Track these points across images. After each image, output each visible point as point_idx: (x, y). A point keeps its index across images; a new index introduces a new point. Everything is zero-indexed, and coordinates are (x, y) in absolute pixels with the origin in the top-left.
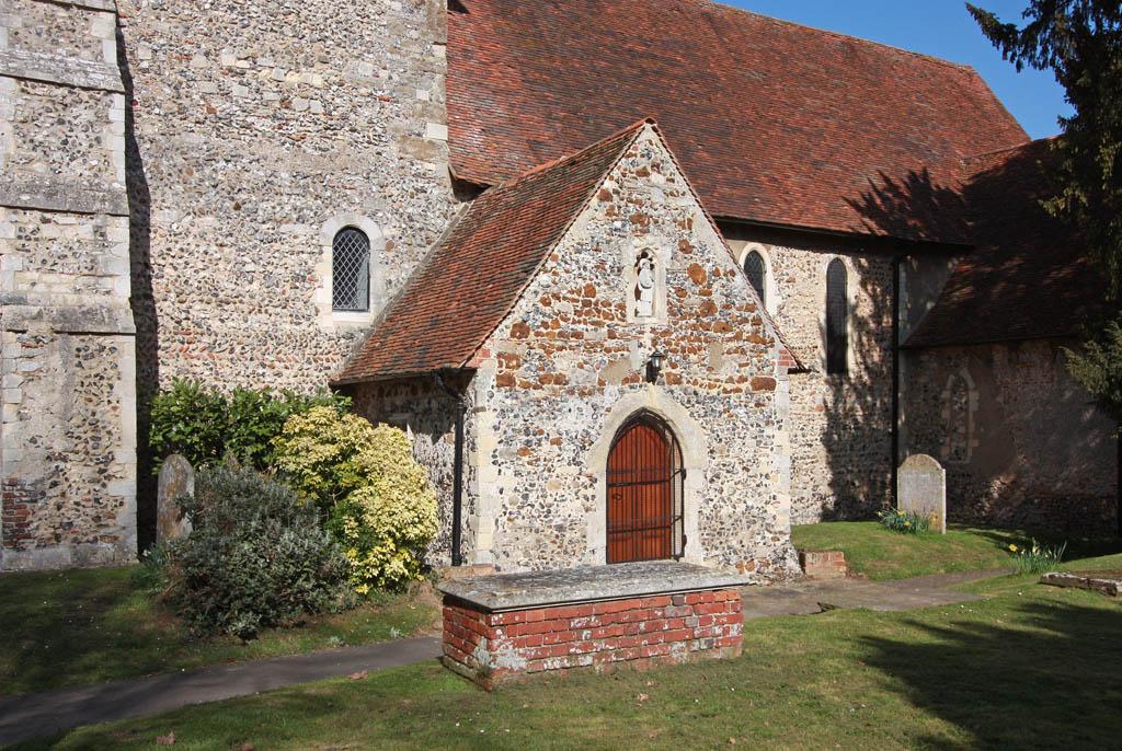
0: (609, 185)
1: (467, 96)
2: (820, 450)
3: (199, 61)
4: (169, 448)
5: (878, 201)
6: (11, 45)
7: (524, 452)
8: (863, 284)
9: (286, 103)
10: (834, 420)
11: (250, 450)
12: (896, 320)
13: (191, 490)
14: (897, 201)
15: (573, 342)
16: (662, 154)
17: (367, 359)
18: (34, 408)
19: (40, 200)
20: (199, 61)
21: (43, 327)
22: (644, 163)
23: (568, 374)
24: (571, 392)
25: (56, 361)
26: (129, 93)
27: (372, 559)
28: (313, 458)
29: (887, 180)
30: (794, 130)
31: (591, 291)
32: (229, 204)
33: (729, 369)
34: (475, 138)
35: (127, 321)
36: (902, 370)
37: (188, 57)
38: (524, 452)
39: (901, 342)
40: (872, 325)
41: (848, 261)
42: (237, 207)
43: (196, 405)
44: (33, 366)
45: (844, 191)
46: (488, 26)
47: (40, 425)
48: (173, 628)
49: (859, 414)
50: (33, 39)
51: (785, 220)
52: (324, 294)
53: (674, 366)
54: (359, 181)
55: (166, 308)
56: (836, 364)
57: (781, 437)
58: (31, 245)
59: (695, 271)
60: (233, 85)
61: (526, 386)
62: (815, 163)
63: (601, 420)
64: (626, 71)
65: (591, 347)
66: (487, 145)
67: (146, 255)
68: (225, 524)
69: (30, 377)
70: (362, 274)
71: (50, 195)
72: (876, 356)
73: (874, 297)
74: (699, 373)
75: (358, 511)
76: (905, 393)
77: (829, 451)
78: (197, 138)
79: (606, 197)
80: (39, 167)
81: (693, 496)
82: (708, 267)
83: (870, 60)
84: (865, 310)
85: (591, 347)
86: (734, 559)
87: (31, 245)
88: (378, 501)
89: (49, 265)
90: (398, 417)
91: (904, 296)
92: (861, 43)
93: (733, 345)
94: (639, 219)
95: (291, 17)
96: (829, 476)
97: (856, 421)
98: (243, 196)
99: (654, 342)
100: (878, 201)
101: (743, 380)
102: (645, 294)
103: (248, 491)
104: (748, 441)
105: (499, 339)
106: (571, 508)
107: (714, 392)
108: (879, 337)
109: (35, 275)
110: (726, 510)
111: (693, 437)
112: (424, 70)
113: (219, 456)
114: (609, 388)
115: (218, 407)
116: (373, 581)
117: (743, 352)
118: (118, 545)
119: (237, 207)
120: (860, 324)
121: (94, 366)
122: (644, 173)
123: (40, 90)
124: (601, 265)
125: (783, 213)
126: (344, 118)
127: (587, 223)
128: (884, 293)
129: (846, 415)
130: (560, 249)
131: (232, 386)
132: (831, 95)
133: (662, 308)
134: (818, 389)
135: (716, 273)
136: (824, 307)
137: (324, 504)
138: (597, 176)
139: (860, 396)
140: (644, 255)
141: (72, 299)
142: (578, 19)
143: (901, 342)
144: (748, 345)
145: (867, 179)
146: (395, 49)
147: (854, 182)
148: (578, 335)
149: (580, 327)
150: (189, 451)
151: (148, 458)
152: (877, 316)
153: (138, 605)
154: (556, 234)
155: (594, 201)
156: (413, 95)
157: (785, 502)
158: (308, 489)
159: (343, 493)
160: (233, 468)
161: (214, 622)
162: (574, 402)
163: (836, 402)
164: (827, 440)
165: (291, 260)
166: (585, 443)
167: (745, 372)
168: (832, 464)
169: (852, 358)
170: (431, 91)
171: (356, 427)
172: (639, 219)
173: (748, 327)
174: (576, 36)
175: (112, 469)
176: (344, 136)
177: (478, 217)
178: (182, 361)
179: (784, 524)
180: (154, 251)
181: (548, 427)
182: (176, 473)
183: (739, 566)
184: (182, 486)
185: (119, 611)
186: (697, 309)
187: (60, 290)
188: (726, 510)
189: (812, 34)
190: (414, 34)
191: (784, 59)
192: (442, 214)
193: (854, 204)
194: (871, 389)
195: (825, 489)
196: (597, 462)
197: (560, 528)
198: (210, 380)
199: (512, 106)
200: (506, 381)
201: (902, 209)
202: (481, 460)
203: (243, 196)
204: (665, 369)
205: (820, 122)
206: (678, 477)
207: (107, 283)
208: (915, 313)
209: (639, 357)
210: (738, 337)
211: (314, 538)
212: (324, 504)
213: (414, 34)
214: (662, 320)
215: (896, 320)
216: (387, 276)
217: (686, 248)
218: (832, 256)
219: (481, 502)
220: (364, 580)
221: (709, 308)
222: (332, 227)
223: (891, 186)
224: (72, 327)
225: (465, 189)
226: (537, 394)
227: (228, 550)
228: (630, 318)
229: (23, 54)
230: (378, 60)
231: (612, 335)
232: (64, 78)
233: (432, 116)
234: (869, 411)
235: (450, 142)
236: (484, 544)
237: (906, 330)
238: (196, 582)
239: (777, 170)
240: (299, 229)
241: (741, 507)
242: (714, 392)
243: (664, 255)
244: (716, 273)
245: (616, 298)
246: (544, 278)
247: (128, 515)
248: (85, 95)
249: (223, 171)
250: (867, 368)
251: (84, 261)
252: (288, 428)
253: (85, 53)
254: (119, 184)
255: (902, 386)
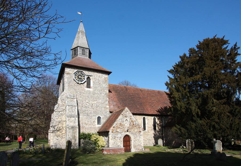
0: (122, 113)
1: (111, 102)
2: (153, 138)
3: (84, 101)
4: (81, 138)
5: (160, 110)
6: (68, 102)
7: (114, 139)
8: (158, 120)
9: (92, 105)
10: (155, 135)
11: (89, 138)
12: (162, 124)
13: (83, 142)
14: (162, 110)
15: (119, 128)
16: (128, 110)
17: (100, 130)
18: (69, 135)
19: (70, 116)
20: (84, 101)
21: (70, 128)
22: (126, 111)
23: (119, 131)
24: (119, 133)
25: (71, 130)
26: (78, 106)
27: (99, 148)
28: (94, 139)
29: (161, 108)
30: (150, 103)
31: (121, 123)
32: (87, 115)
33: (136, 130)
34: (112, 107)
35: (78, 127)
36: (163, 129)
37: (83, 101)
38: (114, 139)
39: (163, 126)
40: (159, 124)
41: (156, 117)
42: (88, 115)
43: (84, 134)
44: (69, 131)
45: (156, 110)
46: (114, 94)
47: (70, 136)
48: (82, 153)
49: (158, 134)
50: (69, 102)
51: (148, 113)
52: (96, 123)
53: (130, 130)
54: (100, 112)
55: (81, 125)
56: (155, 129)
57: (142, 137)
58: (69, 120)
59: (132, 121)
60: (87, 104)
61: (115, 132)
62: (152, 107)
63: (122, 136)
64: (130, 97)
65: (121, 129)
66: (113, 107)
67: (79, 120)
68: (86, 145)
69: (69, 132)
70: (100, 121)
71: (71, 116)
72: (160, 128)
73: (159, 121)
74: (133, 131)
75: (98, 144)
76: (164, 132)
77: (154, 138)
78: (84, 109)
79: (122, 114)
80: (70, 113)
81: (132, 143)
82: (133, 121)
83: (161, 93)
84: (158, 122)
85: (121, 129)
86: (137, 149)
87: (69, 120)
88: (100, 143)
89: (71, 122)
90: (103, 135)
91: (163, 121)
92: (160, 91)
93: (136, 128)
94: (126, 116)
95: (93, 97)
96: (154, 141)
97: (158, 135)
98: (88, 114)
99: (128, 128)
100: (160, 110)
101: (138, 131)
102: (127, 123)
103: (88, 142)
104: (138, 137)
105: (112, 128)
106: (119, 144)
107: (134, 133)
108: (160, 126)
109: (70, 123)
110: (136, 144)
111: (132, 137)
112: (106, 100)
113: (86, 139)
114: (123, 132)
115: (86, 135)
116: (99, 150)
117: (137, 129)
118: (77, 147)
119: (88, 115)
120: (158, 124)
121: (75, 131)
122: (126, 112)
123: (70, 106)
124: (122, 121)
125: (147, 112)
126: (98, 106)
127: (120, 117)
128: (161, 121)
129: (156, 134)
130: (118, 119)
131: (87, 132)
132: (155, 98)
133: (128, 125)
134: (153, 132)
135: (134, 121)
136: (153, 123)
137: (95, 143)
138: (121, 112)
139: (158, 132)
140: (126, 120)
141: (73, 125)
142: (125, 92)
143: (163, 126)
144: (138, 128)
145: (159, 108)
146: (103, 99)
147: (157, 108)
148: (120, 128)
149: (120, 127)
150: (83, 138)
151: (80, 139)
152: (160, 123)
153: (79, 151)
154: (117, 118)
155: (121, 115)
156: (105, 103)
157: (143, 143)
158: (94, 142)
159: (97, 142)
160: (87, 140)
161: (85, 153)
162: (119, 134)
163: (155, 133)
164: (154, 137)
165: (93, 120)
166: (121, 138)
167: (138, 131)
168: (155, 140)
169: (157, 128)
170: (107, 102)
171: (98, 136)
172: (126, 116)
173: (138, 126)
174: (124, 94)
175: (76, 140)
176: (98, 108)
177: (112, 115)
178: (83, 130)
179: (143, 146)
180: (80, 120)
181: (117, 136)
182: (82, 140)
183: (138, 150)
184: (82, 141)
185: (77, 151)
186: (132, 125)
187: (72, 124)
188: (136, 144)
189: (154, 91)
190: (105, 97)
191: (150, 94)
192: (108, 115)
193: (157, 111)
194: (159, 131)
195: (154, 143)
196: (122, 139)
197: (118, 146)
198: (85, 132)
199: (116, 103)
200: (113, 132)
201: (163, 111)
202: (110, 139)
203: (88, 114)
204: (129, 130)
205: (153, 101)
206: (131, 141)
207: (76, 123)
208: (164, 123)
209: (126, 130)
210: (137, 127)
211: (94, 146)
212: (95, 143)
213: (105, 97)
214: (128, 126)
215: (162, 124)
216: (103, 121)
217: (131, 119)
218: (154, 117)
219: (110, 143)
220: (99, 150)
221: (134, 124)
222: (97, 117)
223: (162, 108)
224: (73, 127)
225: (111, 112)
226: (115, 133)
227: (86, 147)
228: (125, 126)
229: (69, 103)
230: (102, 100)
231: (123, 127)
232: (72, 105)
233: (107, 105)
234: (159, 134)
235: (109, 107)
236: (111, 146)
237: (164, 125)
238: (84, 149)
239: (147, 108)
240: (94, 117)
241: (138, 144)
242: (134, 133)
243: (128, 120)
244: (134, 121)
245: (123, 124)
246: (116, 122)
247: (78, 144)
248: (74, 107)
249: (86, 112)
250: (159, 129)
251: (74, 121)
252: (92, 136)
253: (74, 102)
254: (77, 114)
255: (163, 131)
